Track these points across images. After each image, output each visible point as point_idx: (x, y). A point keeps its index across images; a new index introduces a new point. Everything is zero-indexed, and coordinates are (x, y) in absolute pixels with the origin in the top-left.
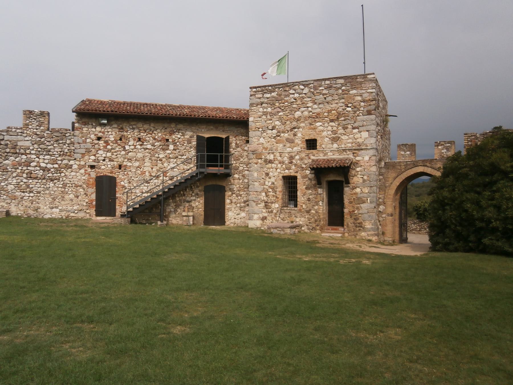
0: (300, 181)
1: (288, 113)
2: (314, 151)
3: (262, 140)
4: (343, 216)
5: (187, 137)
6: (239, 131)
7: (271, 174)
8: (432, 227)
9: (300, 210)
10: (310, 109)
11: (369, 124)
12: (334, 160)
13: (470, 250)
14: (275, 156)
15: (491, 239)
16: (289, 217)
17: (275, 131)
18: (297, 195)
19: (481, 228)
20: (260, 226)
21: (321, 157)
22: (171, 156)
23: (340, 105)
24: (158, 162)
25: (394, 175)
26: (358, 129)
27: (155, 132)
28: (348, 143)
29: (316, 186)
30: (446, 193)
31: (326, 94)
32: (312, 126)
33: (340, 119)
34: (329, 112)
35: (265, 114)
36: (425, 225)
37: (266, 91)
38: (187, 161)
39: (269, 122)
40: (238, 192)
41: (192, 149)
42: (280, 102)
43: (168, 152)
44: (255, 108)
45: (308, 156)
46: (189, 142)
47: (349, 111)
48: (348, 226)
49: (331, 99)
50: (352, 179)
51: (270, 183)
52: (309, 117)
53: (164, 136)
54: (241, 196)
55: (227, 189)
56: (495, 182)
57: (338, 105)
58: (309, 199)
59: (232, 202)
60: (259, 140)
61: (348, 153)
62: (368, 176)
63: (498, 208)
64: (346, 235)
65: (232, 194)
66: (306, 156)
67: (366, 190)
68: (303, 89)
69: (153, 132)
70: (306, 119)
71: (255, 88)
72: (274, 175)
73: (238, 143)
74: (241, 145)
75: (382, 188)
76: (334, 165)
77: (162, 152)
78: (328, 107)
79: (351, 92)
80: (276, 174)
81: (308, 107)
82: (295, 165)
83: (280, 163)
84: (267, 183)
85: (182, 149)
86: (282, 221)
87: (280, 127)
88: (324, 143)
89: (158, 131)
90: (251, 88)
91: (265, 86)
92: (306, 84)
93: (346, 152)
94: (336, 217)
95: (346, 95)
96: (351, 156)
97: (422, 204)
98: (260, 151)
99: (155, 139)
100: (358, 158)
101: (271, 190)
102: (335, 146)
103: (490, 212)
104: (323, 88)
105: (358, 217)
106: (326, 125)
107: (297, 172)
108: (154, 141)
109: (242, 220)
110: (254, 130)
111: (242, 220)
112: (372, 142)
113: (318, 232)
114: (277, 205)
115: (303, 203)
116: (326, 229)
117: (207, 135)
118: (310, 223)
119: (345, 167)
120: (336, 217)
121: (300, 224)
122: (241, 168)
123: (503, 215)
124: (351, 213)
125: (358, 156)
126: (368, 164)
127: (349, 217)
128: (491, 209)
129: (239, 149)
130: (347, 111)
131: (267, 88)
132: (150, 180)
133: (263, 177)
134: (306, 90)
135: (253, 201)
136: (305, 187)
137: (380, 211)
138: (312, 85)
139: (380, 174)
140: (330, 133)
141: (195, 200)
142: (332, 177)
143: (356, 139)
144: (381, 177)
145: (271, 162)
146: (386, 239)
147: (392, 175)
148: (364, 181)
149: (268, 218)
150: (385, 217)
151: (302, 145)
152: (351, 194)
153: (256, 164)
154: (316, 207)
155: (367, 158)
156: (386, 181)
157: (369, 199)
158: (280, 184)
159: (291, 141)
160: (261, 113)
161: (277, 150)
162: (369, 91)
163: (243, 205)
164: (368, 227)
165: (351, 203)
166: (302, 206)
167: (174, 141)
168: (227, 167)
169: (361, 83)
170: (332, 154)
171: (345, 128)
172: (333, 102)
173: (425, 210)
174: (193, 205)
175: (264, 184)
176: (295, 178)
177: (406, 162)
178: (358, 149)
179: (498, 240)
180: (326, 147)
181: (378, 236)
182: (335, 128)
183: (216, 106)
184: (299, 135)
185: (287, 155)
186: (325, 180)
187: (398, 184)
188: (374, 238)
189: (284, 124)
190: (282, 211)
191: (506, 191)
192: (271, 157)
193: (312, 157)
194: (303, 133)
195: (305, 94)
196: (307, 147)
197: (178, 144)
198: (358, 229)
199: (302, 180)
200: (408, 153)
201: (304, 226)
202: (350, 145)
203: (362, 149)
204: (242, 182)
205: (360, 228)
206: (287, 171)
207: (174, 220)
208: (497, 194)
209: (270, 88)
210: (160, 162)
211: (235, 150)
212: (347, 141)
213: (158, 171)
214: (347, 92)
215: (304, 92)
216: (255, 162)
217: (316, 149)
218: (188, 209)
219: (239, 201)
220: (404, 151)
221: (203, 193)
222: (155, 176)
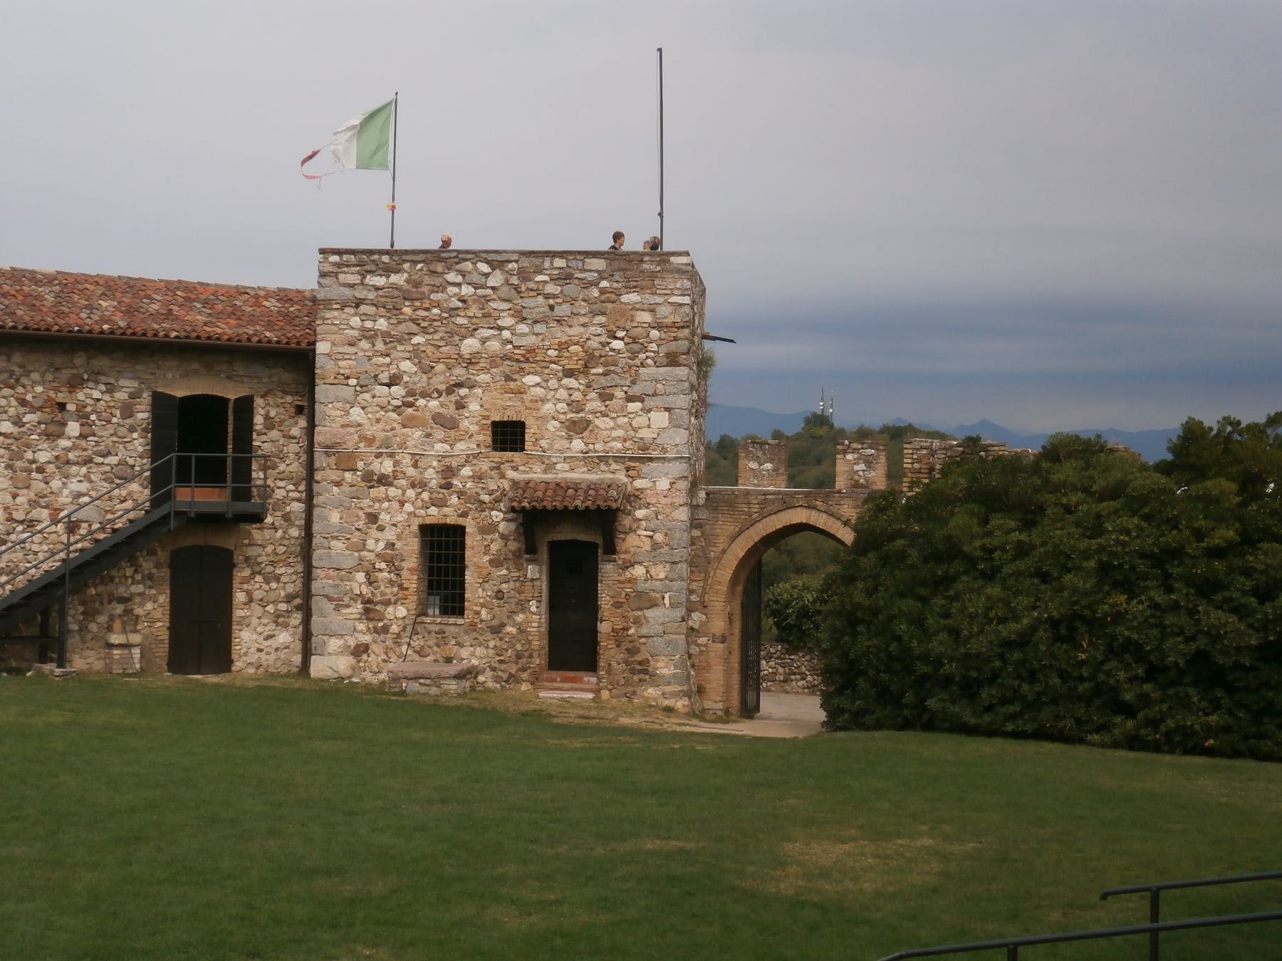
0: (473, 540)
1: (442, 339)
2: (516, 456)
3: (356, 414)
4: (596, 643)
5: (121, 395)
6: (275, 379)
7: (384, 518)
8: (828, 673)
9: (473, 625)
10: (506, 334)
11: (669, 389)
12: (576, 486)
13: (906, 725)
14: (396, 463)
15: (942, 700)
16: (438, 645)
17: (397, 390)
18: (463, 582)
19: (925, 677)
20: (349, 673)
21: (537, 474)
22: (71, 456)
23: (592, 329)
24: (34, 475)
25: (732, 529)
26: (642, 401)
27: (24, 380)
28: (614, 439)
29: (520, 557)
30: (858, 594)
31: (554, 297)
32: (512, 385)
33: (593, 371)
34: (563, 347)
35: (369, 335)
36: (802, 661)
37: (373, 268)
38: (122, 476)
39: (381, 360)
40: (270, 569)
41: (135, 435)
42: (417, 304)
43: (64, 443)
44: (335, 313)
45: (498, 468)
46: (128, 411)
47: (619, 352)
48: (609, 672)
49: (568, 313)
50: (624, 540)
51: (381, 545)
52: (505, 357)
53: (52, 394)
54: (277, 578)
55: (239, 558)
56: (954, 579)
57: (591, 332)
58: (499, 595)
59: (251, 600)
60: (347, 413)
61: (614, 466)
62: (666, 534)
63: (954, 632)
64: (605, 694)
65: (254, 573)
66: (492, 469)
67: (660, 572)
68: (487, 275)
69: (17, 381)
70: (494, 361)
71: (339, 252)
72: (395, 520)
73: (273, 414)
74: (281, 422)
75: (699, 563)
76: (578, 503)
77: (45, 446)
78: (561, 334)
79: (625, 298)
80: (400, 518)
81: (500, 329)
82: (461, 494)
83: (413, 486)
84: (370, 543)
85: (106, 433)
86: (417, 657)
87: (416, 379)
88: (547, 435)
89: (35, 376)
90: (322, 251)
91: (370, 252)
92: (496, 260)
93: (607, 464)
94: (573, 645)
95: (610, 306)
96: (621, 477)
97: (795, 593)
98: (350, 446)
99: (23, 402)
100: (639, 483)
101: (383, 565)
102: (578, 444)
103: (941, 643)
104: (546, 278)
105: (637, 644)
106: (553, 383)
107: (464, 515)
108: (22, 410)
109: (282, 655)
110: (331, 380)
111: (282, 655)
112: (678, 440)
113: (525, 687)
114: (402, 611)
115: (483, 606)
116: (547, 681)
117: (180, 391)
118: (501, 662)
119: (609, 509)
120: (573, 645)
121: (474, 667)
122: (279, 494)
123: (963, 650)
124: (619, 635)
125: (640, 477)
126: (668, 500)
127: (612, 644)
128: (944, 636)
129: (274, 434)
130: (613, 350)
131: (376, 257)
132: (9, 534)
133: (361, 524)
134: (496, 279)
135: (326, 596)
136: (487, 558)
137: (692, 629)
138: (515, 265)
139: (694, 524)
140: (562, 406)
141: (141, 594)
142: (565, 533)
143: (635, 430)
144: (696, 533)
145: (383, 480)
146: (708, 704)
147: (724, 527)
148: (656, 546)
149: (374, 647)
150: (705, 645)
151: (481, 437)
152: (620, 582)
153: (338, 484)
154: (520, 618)
155: (663, 484)
156: (709, 543)
157: (667, 596)
158: (411, 548)
159: (449, 424)
160: (356, 333)
161: (403, 445)
162: (673, 299)
163: (283, 607)
164: (665, 671)
165: (618, 605)
166: (478, 613)
167: (81, 407)
168: (242, 494)
169: (653, 276)
170: (567, 467)
171: (605, 397)
172: (575, 321)
173: (804, 613)
174: (138, 611)
175: (364, 548)
176: (460, 531)
177: (765, 494)
178: (640, 457)
179: (954, 702)
180: (551, 447)
181: (690, 698)
182: (577, 396)
183: (173, 276)
184: (474, 406)
185: (435, 463)
186: (544, 541)
187: (741, 554)
188: (681, 704)
189: (428, 370)
190: (419, 628)
191: (970, 600)
192: (387, 466)
193: (511, 474)
194: (482, 405)
195: (493, 288)
196: (494, 441)
197: (93, 417)
198: (636, 678)
199: (479, 538)
200: (769, 466)
201: (483, 671)
202: (620, 446)
203: (651, 459)
204: (283, 538)
205: (642, 676)
206: (433, 510)
207: (83, 660)
208: (955, 604)
209: (385, 259)
210: (39, 476)
211: (264, 438)
212: (611, 432)
213: (33, 504)
214: (613, 297)
215: (491, 282)
216: (334, 478)
217: (523, 449)
218: (124, 623)
219: (272, 596)
220: (757, 459)
221: (165, 573)
222: (22, 522)
